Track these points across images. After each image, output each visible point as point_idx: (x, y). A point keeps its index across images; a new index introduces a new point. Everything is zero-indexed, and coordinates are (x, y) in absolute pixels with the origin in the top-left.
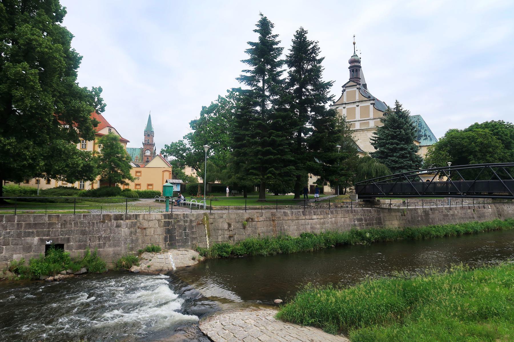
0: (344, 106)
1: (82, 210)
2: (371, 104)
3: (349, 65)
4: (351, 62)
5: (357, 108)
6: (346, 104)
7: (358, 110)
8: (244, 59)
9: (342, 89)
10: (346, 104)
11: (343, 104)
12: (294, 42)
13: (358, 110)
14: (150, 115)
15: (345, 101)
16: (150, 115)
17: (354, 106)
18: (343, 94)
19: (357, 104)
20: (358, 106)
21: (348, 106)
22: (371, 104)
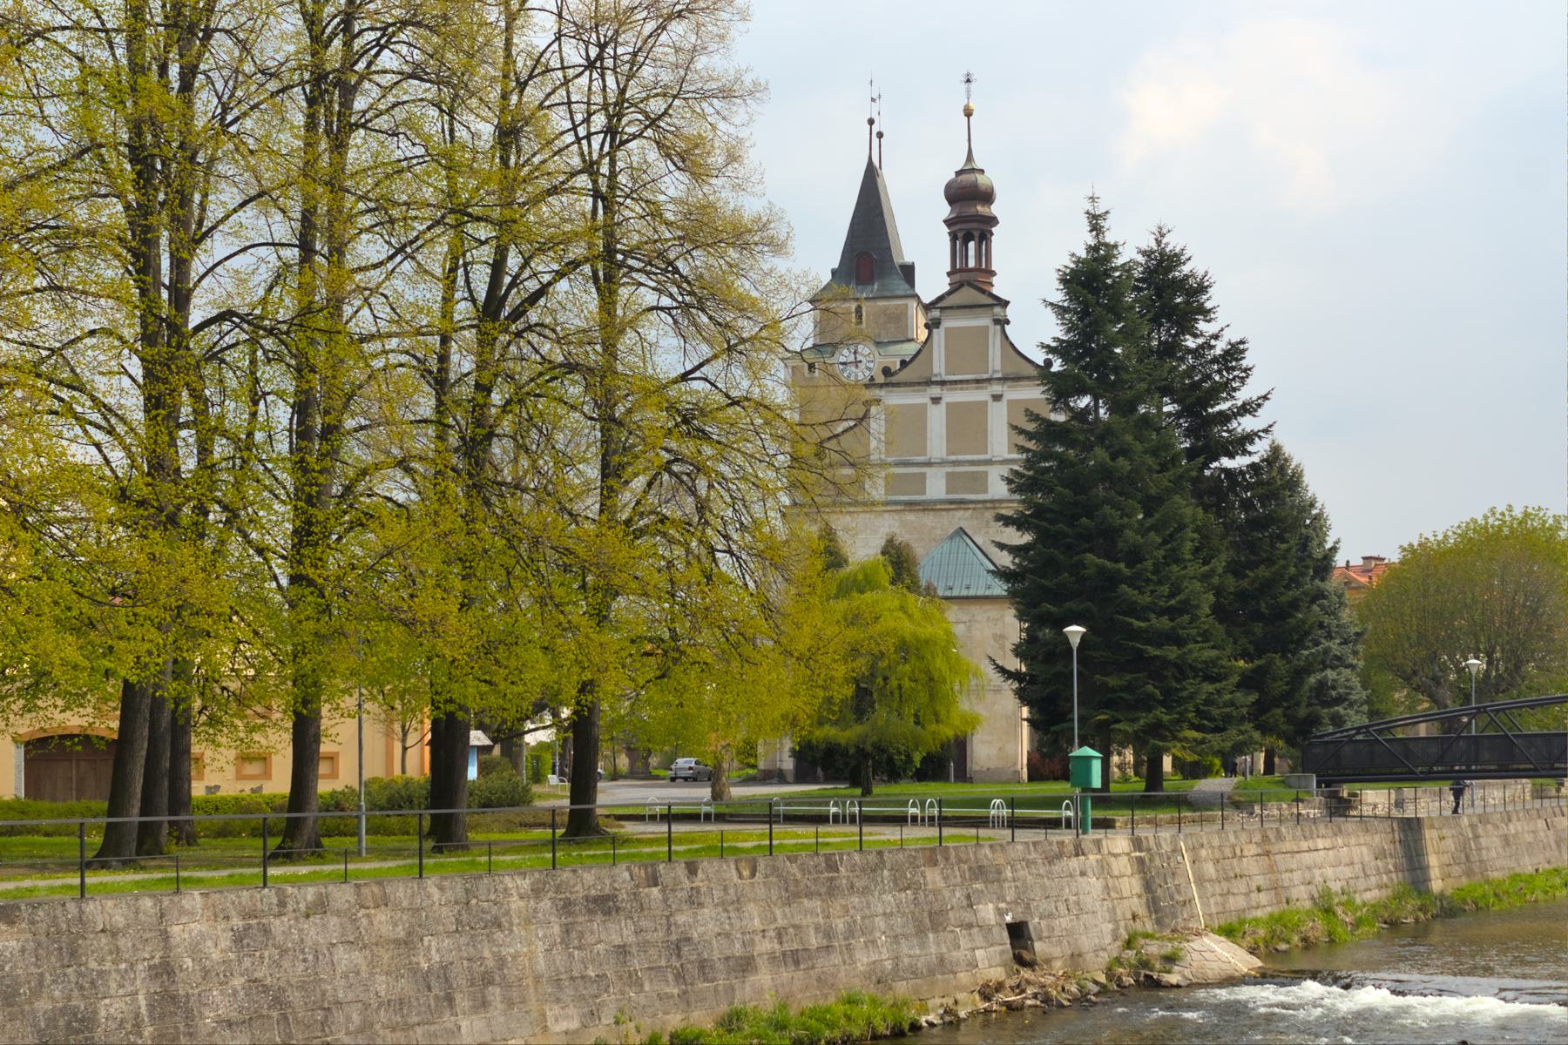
0: (935, 391)
6: (943, 383)
7: (937, 419)
10: (943, 383)
11: (929, 383)
14: (871, 176)
16: (871, 176)
17: (982, 395)
18: (968, 91)
19: (997, 388)
20: (997, 398)
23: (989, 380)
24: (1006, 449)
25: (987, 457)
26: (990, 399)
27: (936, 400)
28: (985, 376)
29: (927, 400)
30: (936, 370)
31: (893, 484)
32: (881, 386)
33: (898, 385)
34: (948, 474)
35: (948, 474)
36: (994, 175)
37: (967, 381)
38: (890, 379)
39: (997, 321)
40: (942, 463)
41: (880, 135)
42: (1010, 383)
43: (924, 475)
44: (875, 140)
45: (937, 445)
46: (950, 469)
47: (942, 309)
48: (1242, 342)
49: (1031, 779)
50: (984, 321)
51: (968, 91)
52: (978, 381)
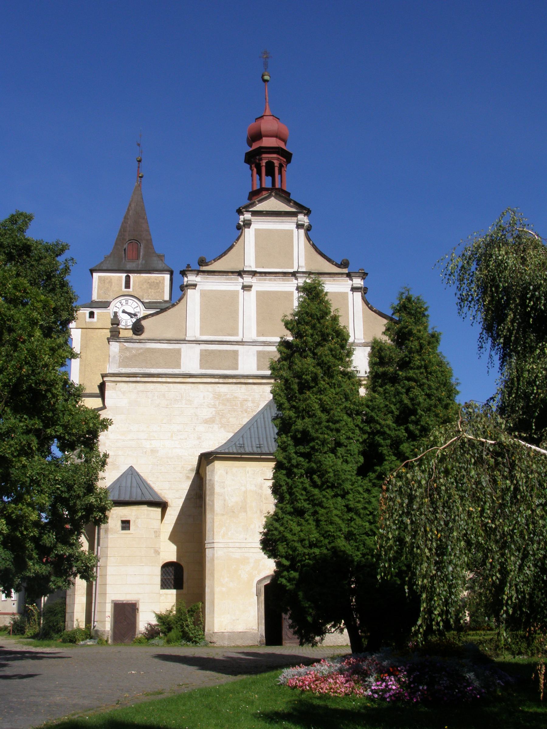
0: (247, 280)
6: (254, 273)
10: (254, 273)
11: (240, 273)
15: (250, 264)
21: (260, 285)
22: (354, 289)
27: (246, 288)
28: (291, 270)
31: (205, 357)
40: (254, 343)
43: (236, 353)
46: (260, 348)
52: (285, 274)
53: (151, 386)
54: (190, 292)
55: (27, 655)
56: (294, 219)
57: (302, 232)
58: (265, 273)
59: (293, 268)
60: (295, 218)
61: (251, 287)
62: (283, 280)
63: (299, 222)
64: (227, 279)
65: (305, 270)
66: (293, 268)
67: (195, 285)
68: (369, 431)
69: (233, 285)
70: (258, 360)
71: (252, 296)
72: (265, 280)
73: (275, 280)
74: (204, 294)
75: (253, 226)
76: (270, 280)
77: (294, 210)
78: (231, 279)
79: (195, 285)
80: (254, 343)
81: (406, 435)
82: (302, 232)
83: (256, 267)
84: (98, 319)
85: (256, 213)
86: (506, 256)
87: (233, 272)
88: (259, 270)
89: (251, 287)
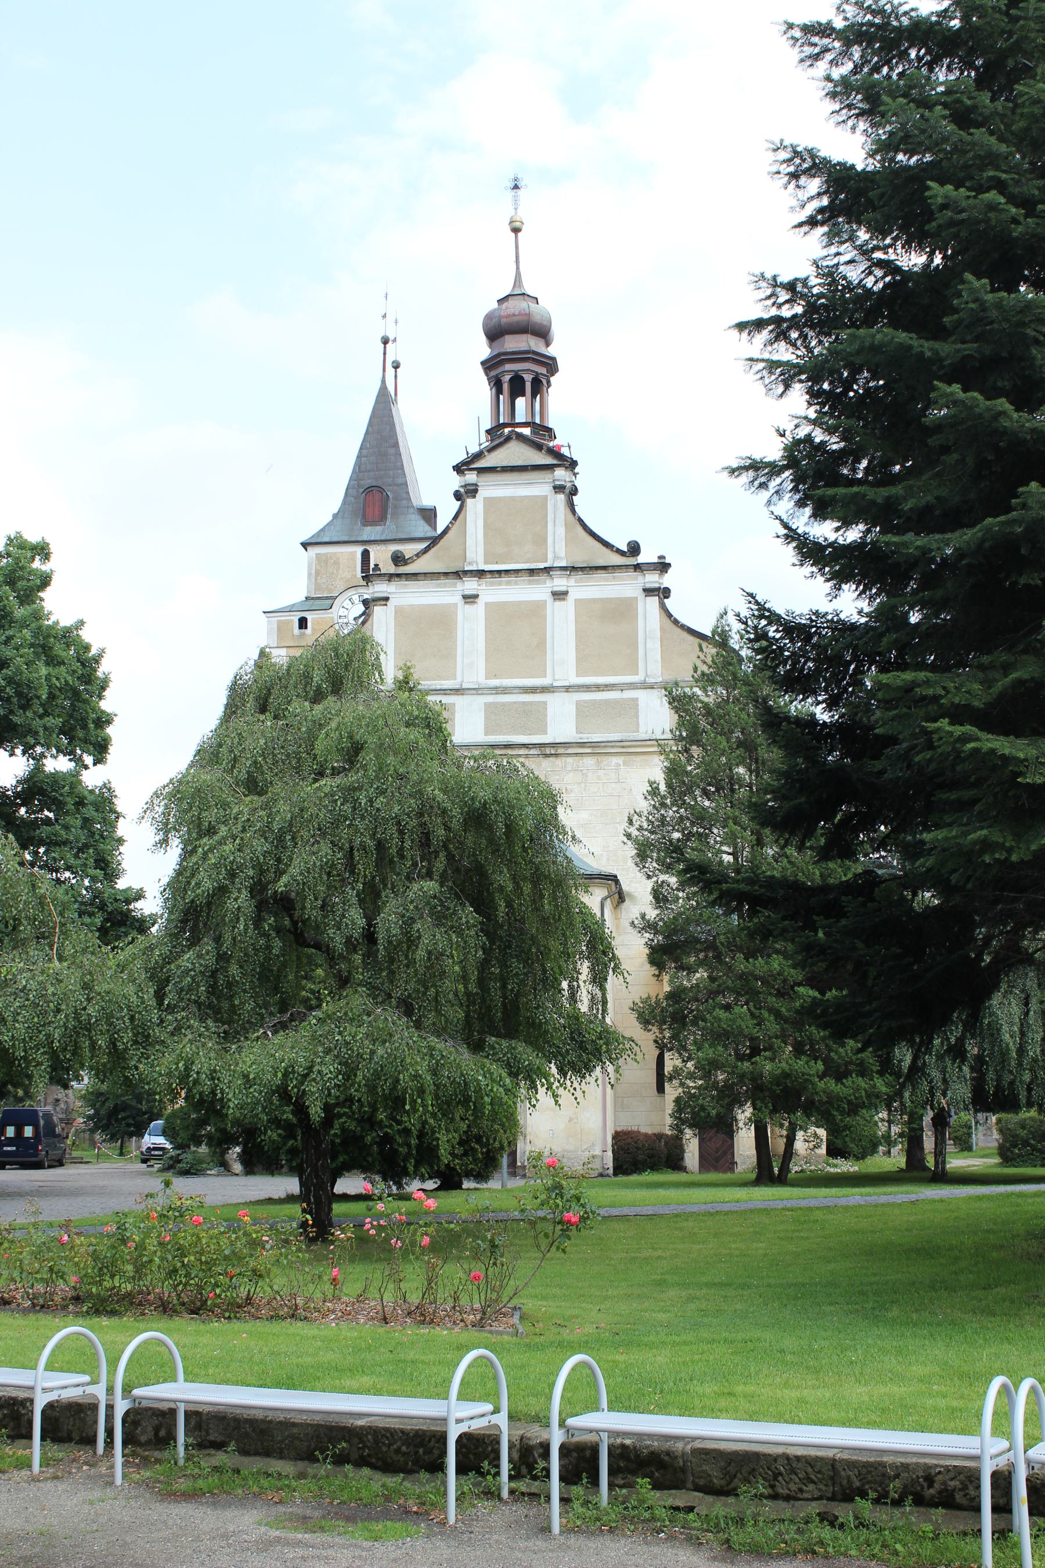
0: (470, 585)
1: (953, 796)
2: (649, 592)
3: (485, 351)
4: (495, 331)
5: (464, 611)
6: (480, 574)
7: (562, 621)
8: (796, 223)
9: (456, 482)
11: (459, 574)
12: (849, 200)
13: (562, 621)
14: (384, 406)
15: (477, 559)
16: (384, 406)
17: (538, 591)
18: (516, 201)
19: (560, 583)
20: (559, 595)
21: (491, 593)
22: (649, 592)
23: (547, 570)
24: (573, 670)
25: (545, 682)
26: (549, 598)
27: (470, 598)
28: (542, 566)
29: (458, 599)
30: (470, 555)
32: (391, 577)
33: (414, 576)
34: (487, 706)
35: (487, 706)
36: (552, 303)
37: (517, 572)
38: (402, 570)
39: (559, 489)
40: (477, 691)
41: (396, 366)
42: (580, 576)
44: (390, 371)
45: (562, 662)
46: (491, 699)
47: (481, 471)
48: (794, 565)
49: (615, 1174)
50: (538, 487)
51: (516, 201)
52: (532, 572)
53: (559, 762)
54: (378, 610)
55: (156, 1153)
56: (546, 476)
57: (561, 497)
58: (499, 572)
59: (546, 561)
60: (550, 476)
61: (476, 596)
62: (530, 583)
63: (557, 483)
64: (438, 586)
65: (564, 565)
66: (546, 561)
67: (387, 599)
68: (391, 1286)
69: (445, 595)
70: (487, 718)
71: (478, 609)
72: (500, 584)
73: (516, 583)
74: (399, 611)
75: (482, 493)
76: (508, 583)
77: (555, 462)
78: (445, 585)
79: (387, 599)
80: (477, 691)
81: (985, 281)
82: (561, 497)
83: (486, 563)
84: (313, 629)
85: (481, 471)
86: (940, 402)
87: (446, 574)
88: (487, 568)
89: (566, 593)
